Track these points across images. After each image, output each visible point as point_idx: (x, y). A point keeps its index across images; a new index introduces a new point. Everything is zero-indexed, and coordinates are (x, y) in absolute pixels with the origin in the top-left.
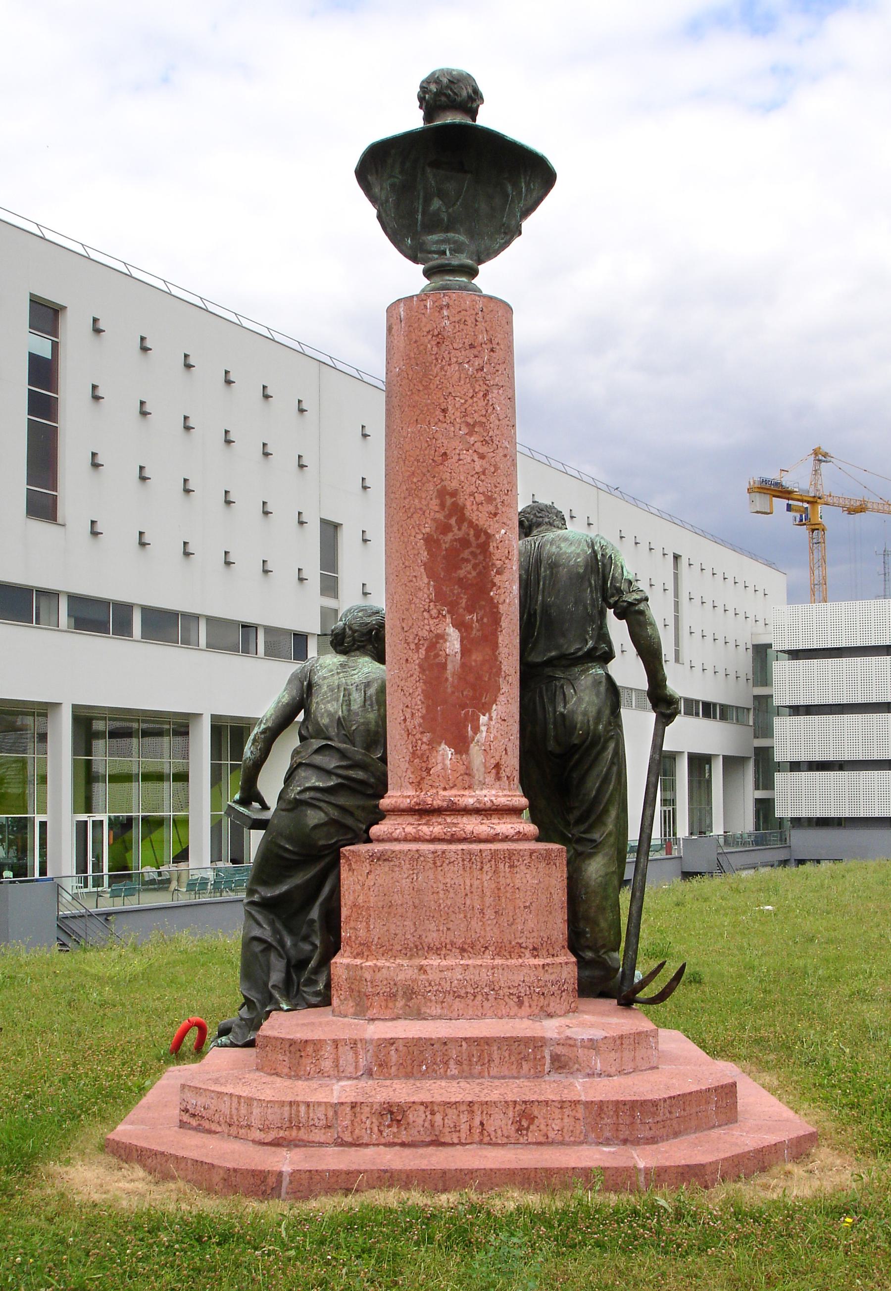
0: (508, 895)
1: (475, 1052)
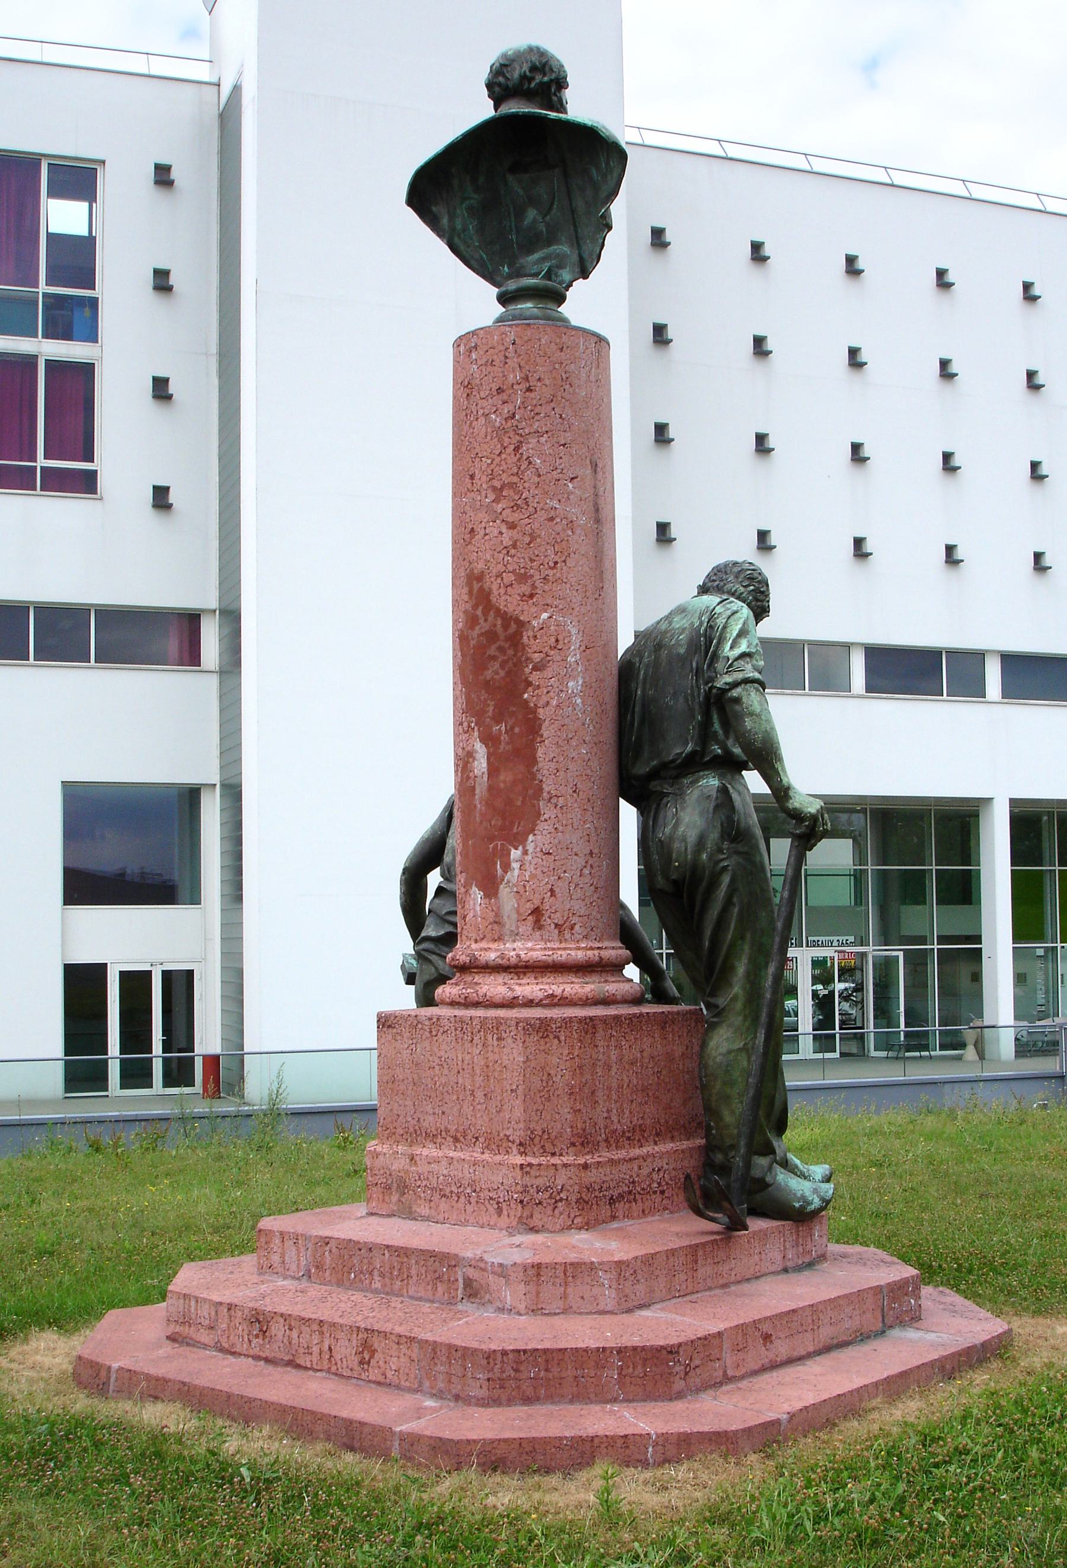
0: (496, 1074)
1: (396, 1264)
